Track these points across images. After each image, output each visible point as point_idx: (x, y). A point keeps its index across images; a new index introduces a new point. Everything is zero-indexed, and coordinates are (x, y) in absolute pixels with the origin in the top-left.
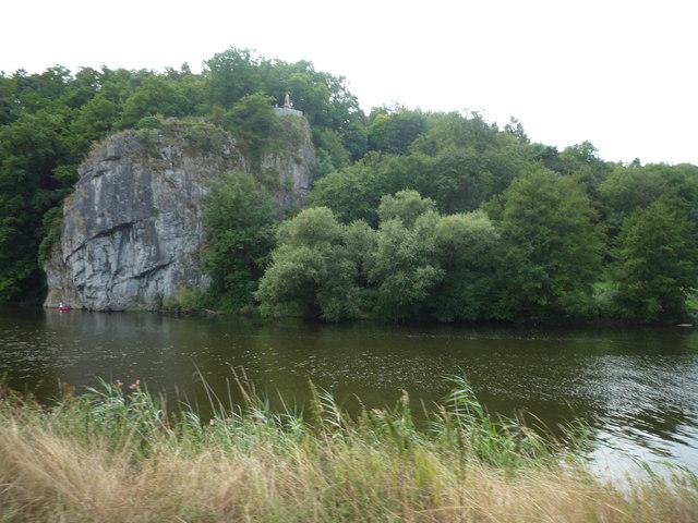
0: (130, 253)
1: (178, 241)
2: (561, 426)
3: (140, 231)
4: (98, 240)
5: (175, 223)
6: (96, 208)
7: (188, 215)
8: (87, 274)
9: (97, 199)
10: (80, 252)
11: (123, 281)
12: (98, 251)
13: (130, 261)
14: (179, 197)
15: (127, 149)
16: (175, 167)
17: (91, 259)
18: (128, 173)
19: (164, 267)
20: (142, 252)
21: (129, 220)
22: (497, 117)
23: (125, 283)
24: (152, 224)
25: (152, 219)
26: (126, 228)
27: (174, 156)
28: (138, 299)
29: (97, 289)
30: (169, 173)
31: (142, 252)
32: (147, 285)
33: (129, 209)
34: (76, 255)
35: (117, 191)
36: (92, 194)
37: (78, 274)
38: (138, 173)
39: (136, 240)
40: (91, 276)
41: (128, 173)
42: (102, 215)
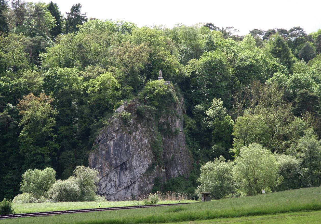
5: (138, 159)
6: (112, 156)
8: (108, 188)
9: (112, 151)
22: (282, 28)
27: (134, 124)
29: (111, 195)
31: (128, 175)
34: (103, 179)
36: (109, 149)
42: (116, 159)
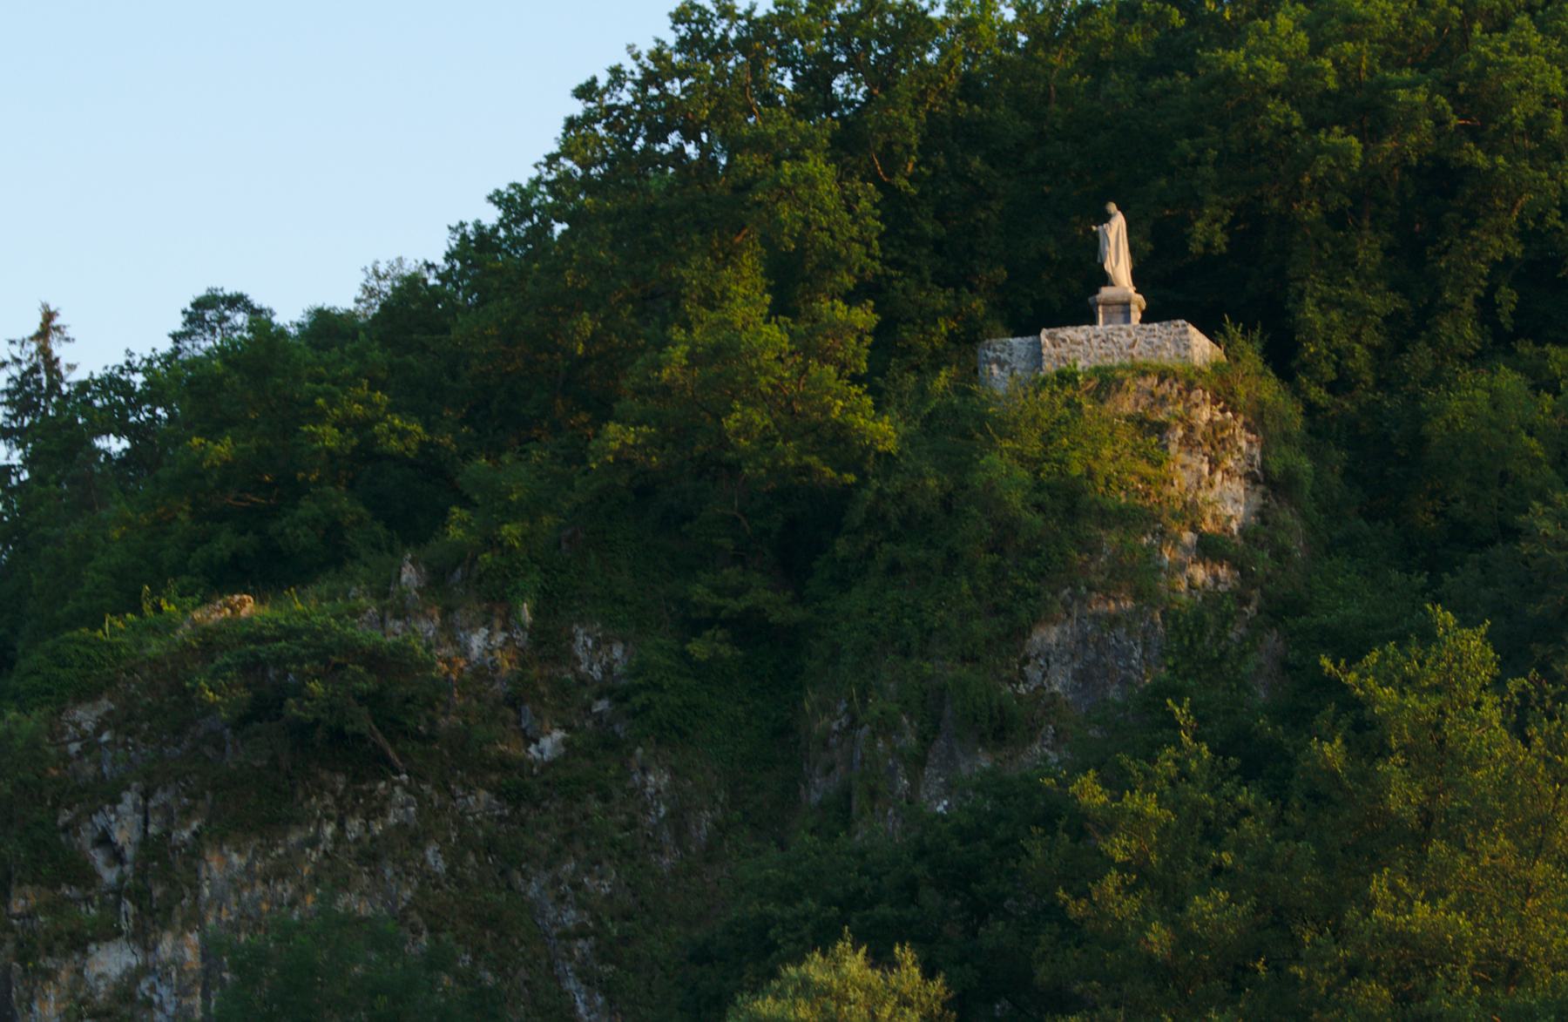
27: (154, 849)
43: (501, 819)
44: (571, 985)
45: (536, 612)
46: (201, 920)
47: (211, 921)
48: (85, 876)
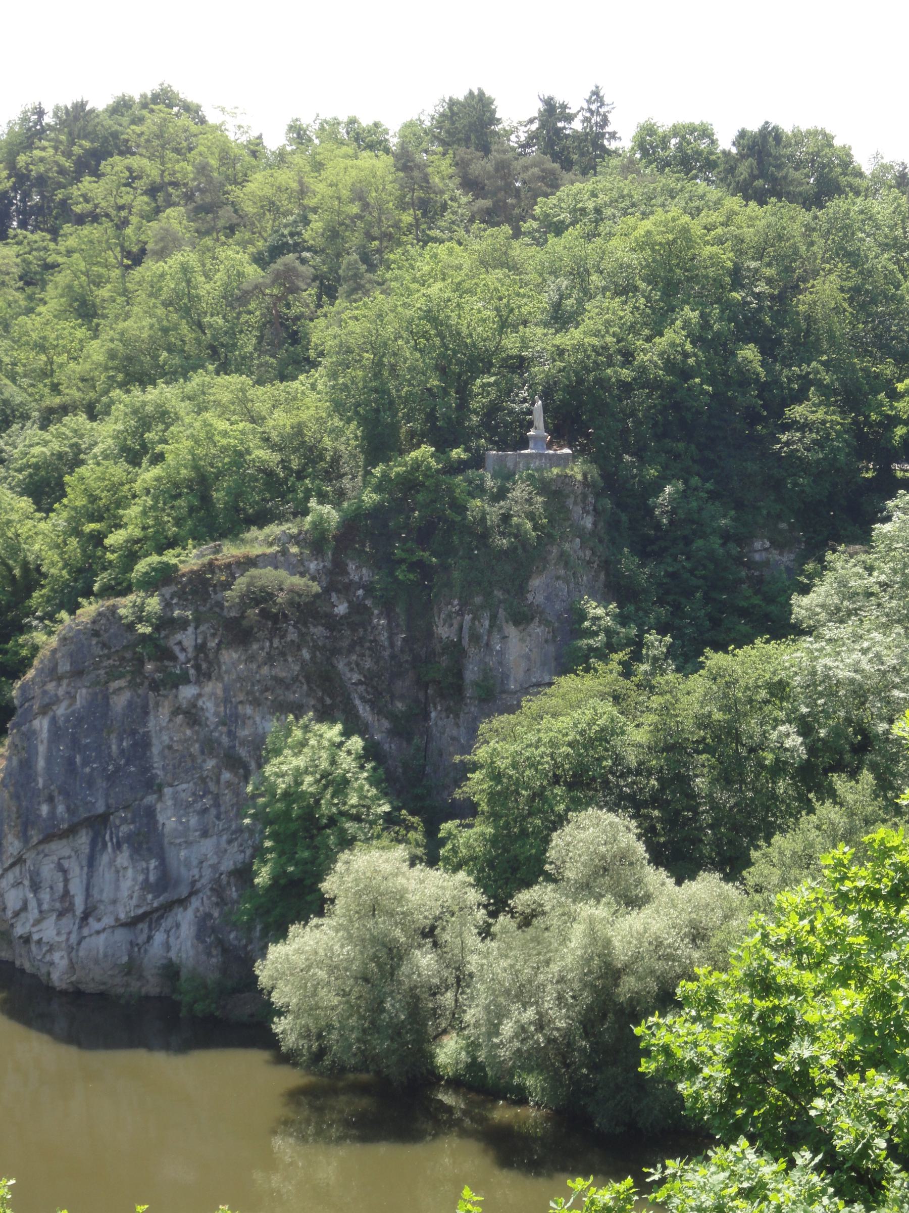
0: (109, 876)
1: (207, 846)
2: (648, 1180)
3: (124, 829)
4: (47, 848)
5: (198, 806)
7: (229, 784)
10: (17, 869)
11: (98, 932)
12: (47, 870)
13: (107, 895)
14: (209, 746)
15: (98, 651)
16: (203, 676)
17: (35, 887)
18: (100, 703)
19: (182, 902)
20: (130, 873)
21: (100, 808)
23: (103, 936)
24: (150, 813)
25: (151, 799)
26: (98, 824)
27: (201, 648)
28: (132, 968)
30: (187, 692)
31: (130, 873)
32: (150, 938)
33: (101, 783)
35: (75, 744)
37: (17, 914)
38: (120, 702)
39: (118, 846)
40: (37, 922)
41: (100, 703)
42: (51, 799)
43: (327, 637)
44: (357, 702)
45: (333, 555)
46: (222, 678)
47: (226, 679)
48: (174, 658)
